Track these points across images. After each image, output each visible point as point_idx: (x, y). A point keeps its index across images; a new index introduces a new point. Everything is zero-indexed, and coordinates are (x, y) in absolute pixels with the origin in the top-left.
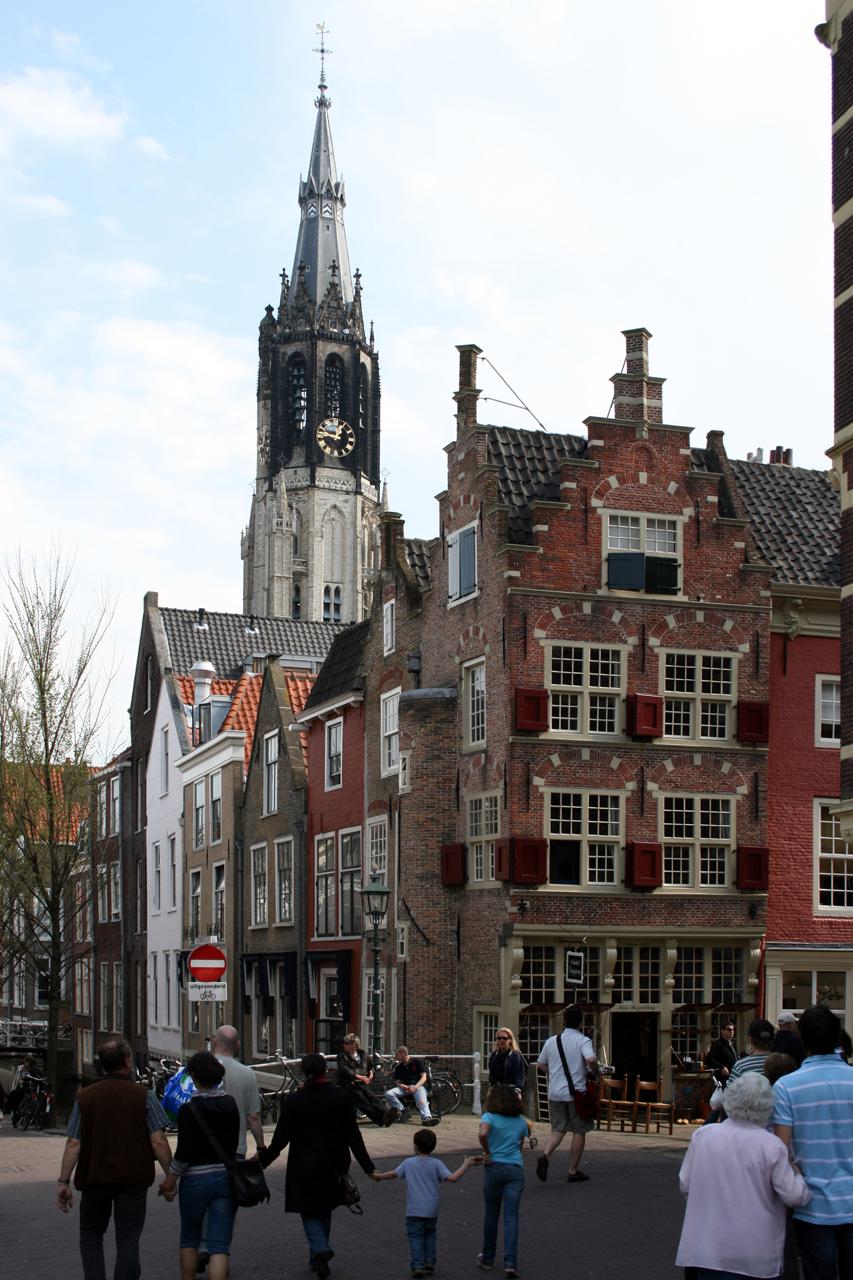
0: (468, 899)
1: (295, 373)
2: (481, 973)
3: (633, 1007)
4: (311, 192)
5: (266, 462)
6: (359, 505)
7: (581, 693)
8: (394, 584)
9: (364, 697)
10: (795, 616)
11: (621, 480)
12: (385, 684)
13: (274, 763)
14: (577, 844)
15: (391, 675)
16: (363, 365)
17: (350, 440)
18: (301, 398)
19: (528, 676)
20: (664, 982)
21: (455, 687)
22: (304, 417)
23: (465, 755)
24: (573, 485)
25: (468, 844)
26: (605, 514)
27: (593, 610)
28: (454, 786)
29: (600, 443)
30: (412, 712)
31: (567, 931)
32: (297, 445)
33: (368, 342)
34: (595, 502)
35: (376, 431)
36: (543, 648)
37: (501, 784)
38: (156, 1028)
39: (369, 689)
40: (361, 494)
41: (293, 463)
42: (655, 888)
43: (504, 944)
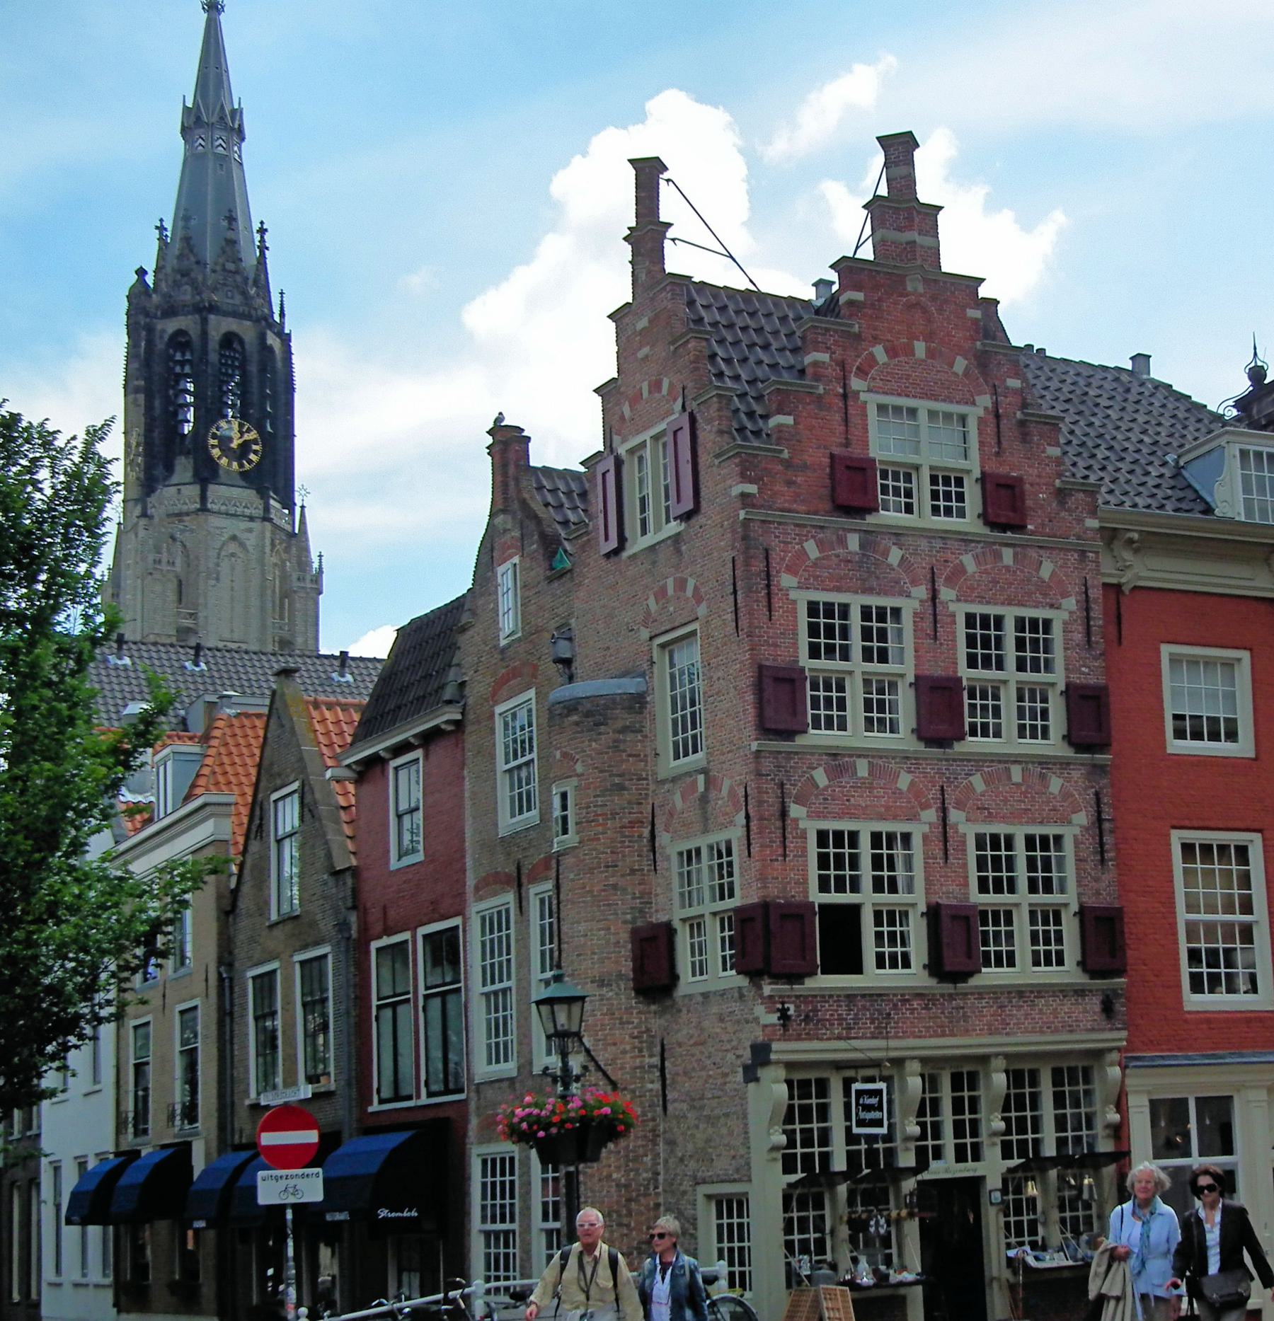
0: (680, 1011)
1: (178, 357)
2: (710, 1131)
3: (947, 1171)
4: (198, 120)
5: (138, 479)
6: (268, 535)
7: (851, 673)
8: (517, 534)
9: (463, 714)
10: (1128, 555)
11: (892, 352)
12: (501, 687)
13: (291, 835)
14: (855, 909)
15: (515, 673)
16: (270, 349)
17: (255, 447)
18: (188, 392)
19: (775, 645)
20: (989, 1127)
21: (643, 675)
22: (191, 416)
23: (663, 782)
24: (824, 357)
25: (677, 924)
26: (872, 401)
27: (862, 546)
28: (646, 832)
29: (859, 296)
30: (575, 718)
31: (861, 1050)
32: (181, 453)
33: (277, 318)
34: (856, 384)
35: (290, 436)
36: (794, 602)
37: (740, 819)
38: (59, 1285)
39: (471, 701)
40: (270, 520)
41: (175, 479)
42: (970, 974)
43: (751, 1075)
